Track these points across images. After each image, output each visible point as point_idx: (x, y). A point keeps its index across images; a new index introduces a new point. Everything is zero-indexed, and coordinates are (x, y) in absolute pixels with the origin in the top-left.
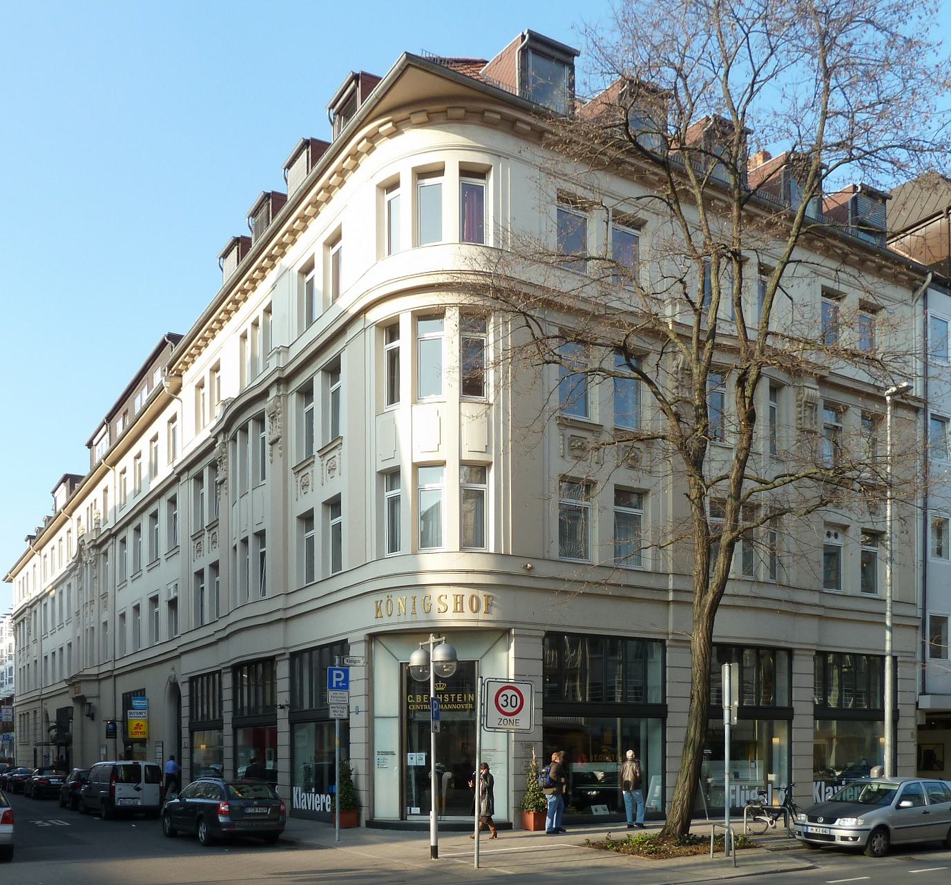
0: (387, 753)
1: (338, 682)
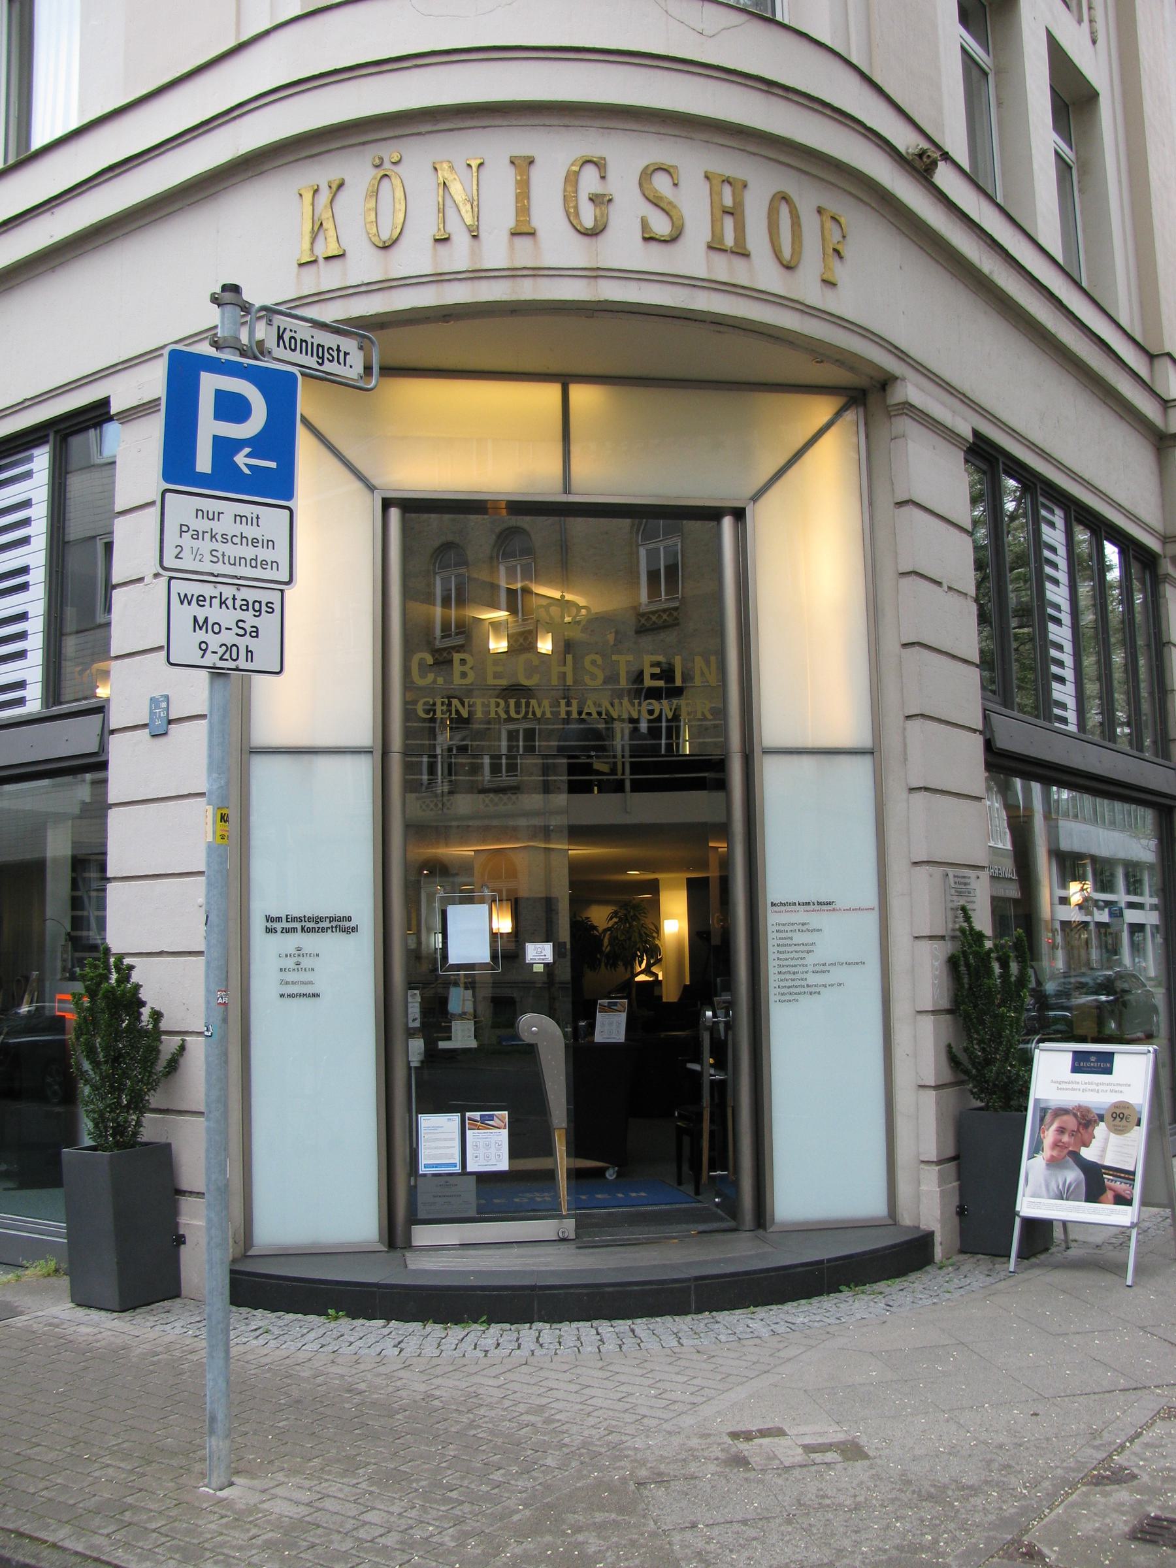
0: (312, 924)
1: (224, 448)
